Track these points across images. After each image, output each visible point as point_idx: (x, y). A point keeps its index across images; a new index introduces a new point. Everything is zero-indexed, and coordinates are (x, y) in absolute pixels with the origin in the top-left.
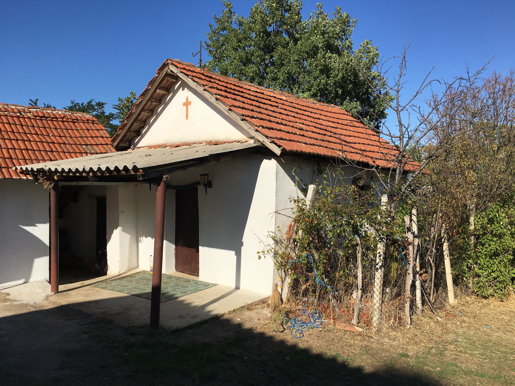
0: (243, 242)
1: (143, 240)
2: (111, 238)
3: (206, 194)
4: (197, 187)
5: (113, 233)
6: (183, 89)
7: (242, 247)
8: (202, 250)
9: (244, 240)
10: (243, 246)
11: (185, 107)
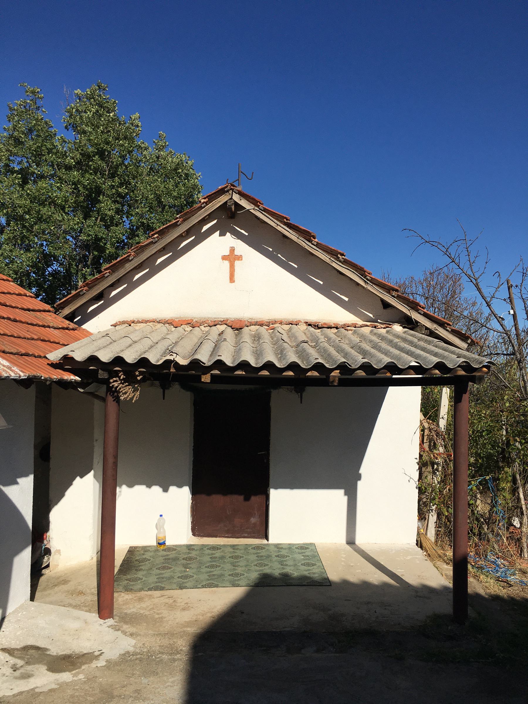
0: (360, 474)
1: (120, 492)
2: (62, 495)
3: (301, 403)
4: (270, 392)
5: (70, 484)
6: (222, 234)
7: (359, 483)
8: (274, 494)
9: (363, 470)
10: (81, 477)
11: (227, 263)
